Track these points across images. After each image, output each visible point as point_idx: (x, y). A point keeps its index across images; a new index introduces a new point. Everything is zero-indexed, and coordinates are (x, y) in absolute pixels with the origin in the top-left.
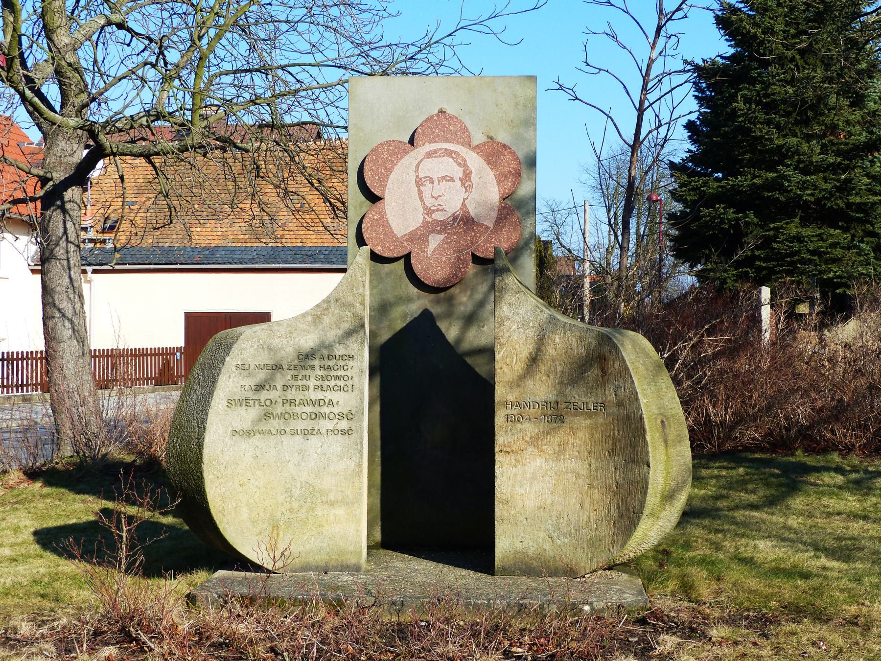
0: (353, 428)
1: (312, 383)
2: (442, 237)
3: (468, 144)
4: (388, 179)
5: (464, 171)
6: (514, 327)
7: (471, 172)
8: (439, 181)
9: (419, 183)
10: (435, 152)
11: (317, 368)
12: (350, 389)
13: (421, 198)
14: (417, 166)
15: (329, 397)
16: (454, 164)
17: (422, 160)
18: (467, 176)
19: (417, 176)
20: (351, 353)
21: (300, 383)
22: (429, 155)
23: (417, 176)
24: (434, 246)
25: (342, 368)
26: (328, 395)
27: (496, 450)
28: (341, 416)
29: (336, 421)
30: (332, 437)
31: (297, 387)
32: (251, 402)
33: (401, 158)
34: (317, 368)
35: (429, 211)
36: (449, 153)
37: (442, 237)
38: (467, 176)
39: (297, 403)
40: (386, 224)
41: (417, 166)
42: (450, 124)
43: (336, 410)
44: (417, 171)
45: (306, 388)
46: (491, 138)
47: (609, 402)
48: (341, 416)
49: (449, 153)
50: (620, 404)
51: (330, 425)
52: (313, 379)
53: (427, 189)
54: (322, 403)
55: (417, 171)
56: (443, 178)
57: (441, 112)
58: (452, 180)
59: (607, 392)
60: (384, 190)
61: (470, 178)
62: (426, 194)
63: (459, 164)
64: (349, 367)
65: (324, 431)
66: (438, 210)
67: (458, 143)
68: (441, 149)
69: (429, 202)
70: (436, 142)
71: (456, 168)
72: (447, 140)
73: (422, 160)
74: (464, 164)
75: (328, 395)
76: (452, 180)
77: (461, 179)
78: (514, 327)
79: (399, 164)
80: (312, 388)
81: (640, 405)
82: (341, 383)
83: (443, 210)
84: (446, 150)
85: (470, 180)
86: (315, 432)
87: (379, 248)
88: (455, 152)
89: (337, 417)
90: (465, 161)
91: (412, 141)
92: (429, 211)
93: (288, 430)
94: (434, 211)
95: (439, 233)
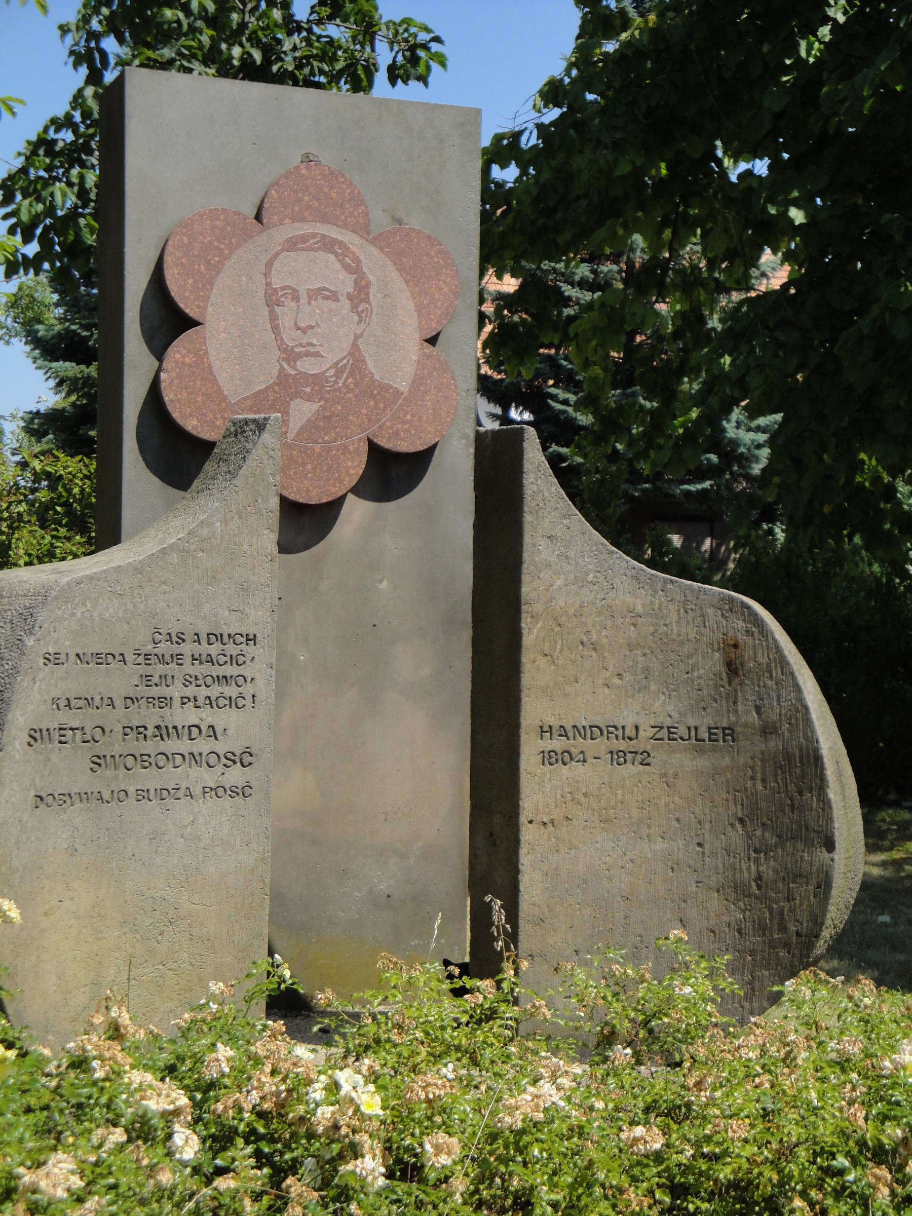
0: (252, 784)
1: (176, 691)
2: (315, 406)
3: (363, 229)
4: (212, 285)
5: (356, 282)
6: (559, 583)
7: (369, 284)
8: (310, 297)
9: (272, 299)
10: (303, 239)
11: (187, 660)
12: (249, 703)
13: (275, 329)
14: (269, 265)
15: (210, 721)
16: (338, 266)
17: (277, 255)
18: (360, 294)
19: (268, 284)
20: (252, 631)
21: (155, 692)
22: (292, 245)
23: (268, 284)
24: (300, 424)
25: (233, 660)
26: (207, 716)
27: (523, 819)
28: (231, 759)
29: (220, 769)
30: (212, 801)
31: (150, 700)
32: (629, 756)
33: (238, 246)
34: (187, 660)
35: (290, 356)
36: (328, 244)
37: (315, 406)
38: (360, 294)
39: (149, 733)
40: (209, 377)
41: (269, 265)
42: (332, 187)
43: (221, 747)
44: (267, 274)
45: (164, 702)
46: (399, 221)
47: (746, 725)
48: (231, 759)
49: (328, 244)
50: (767, 730)
51: (209, 778)
52: (178, 683)
53: (286, 314)
54: (195, 731)
55: (267, 274)
56: (319, 291)
57: (307, 159)
58: (334, 296)
59: (740, 707)
60: (205, 308)
61: (367, 294)
62: (286, 320)
63: (347, 268)
64: (248, 658)
65: (197, 791)
66: (307, 354)
67: (345, 226)
68: (314, 235)
69: (290, 337)
70: (304, 220)
71: (342, 275)
72: (324, 219)
73: (277, 255)
74: (355, 269)
75: (207, 716)
76: (334, 296)
77: (350, 297)
78: (559, 583)
79: (234, 257)
80: (177, 702)
81: (813, 731)
82: (231, 691)
83: (317, 355)
84: (323, 237)
85: (367, 300)
86: (181, 794)
87: (195, 422)
88: (341, 243)
89: (224, 760)
90: (357, 260)
91: (258, 217)
92: (290, 356)
93: (131, 790)
94: (300, 356)
95: (309, 398)
